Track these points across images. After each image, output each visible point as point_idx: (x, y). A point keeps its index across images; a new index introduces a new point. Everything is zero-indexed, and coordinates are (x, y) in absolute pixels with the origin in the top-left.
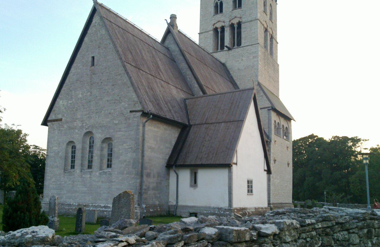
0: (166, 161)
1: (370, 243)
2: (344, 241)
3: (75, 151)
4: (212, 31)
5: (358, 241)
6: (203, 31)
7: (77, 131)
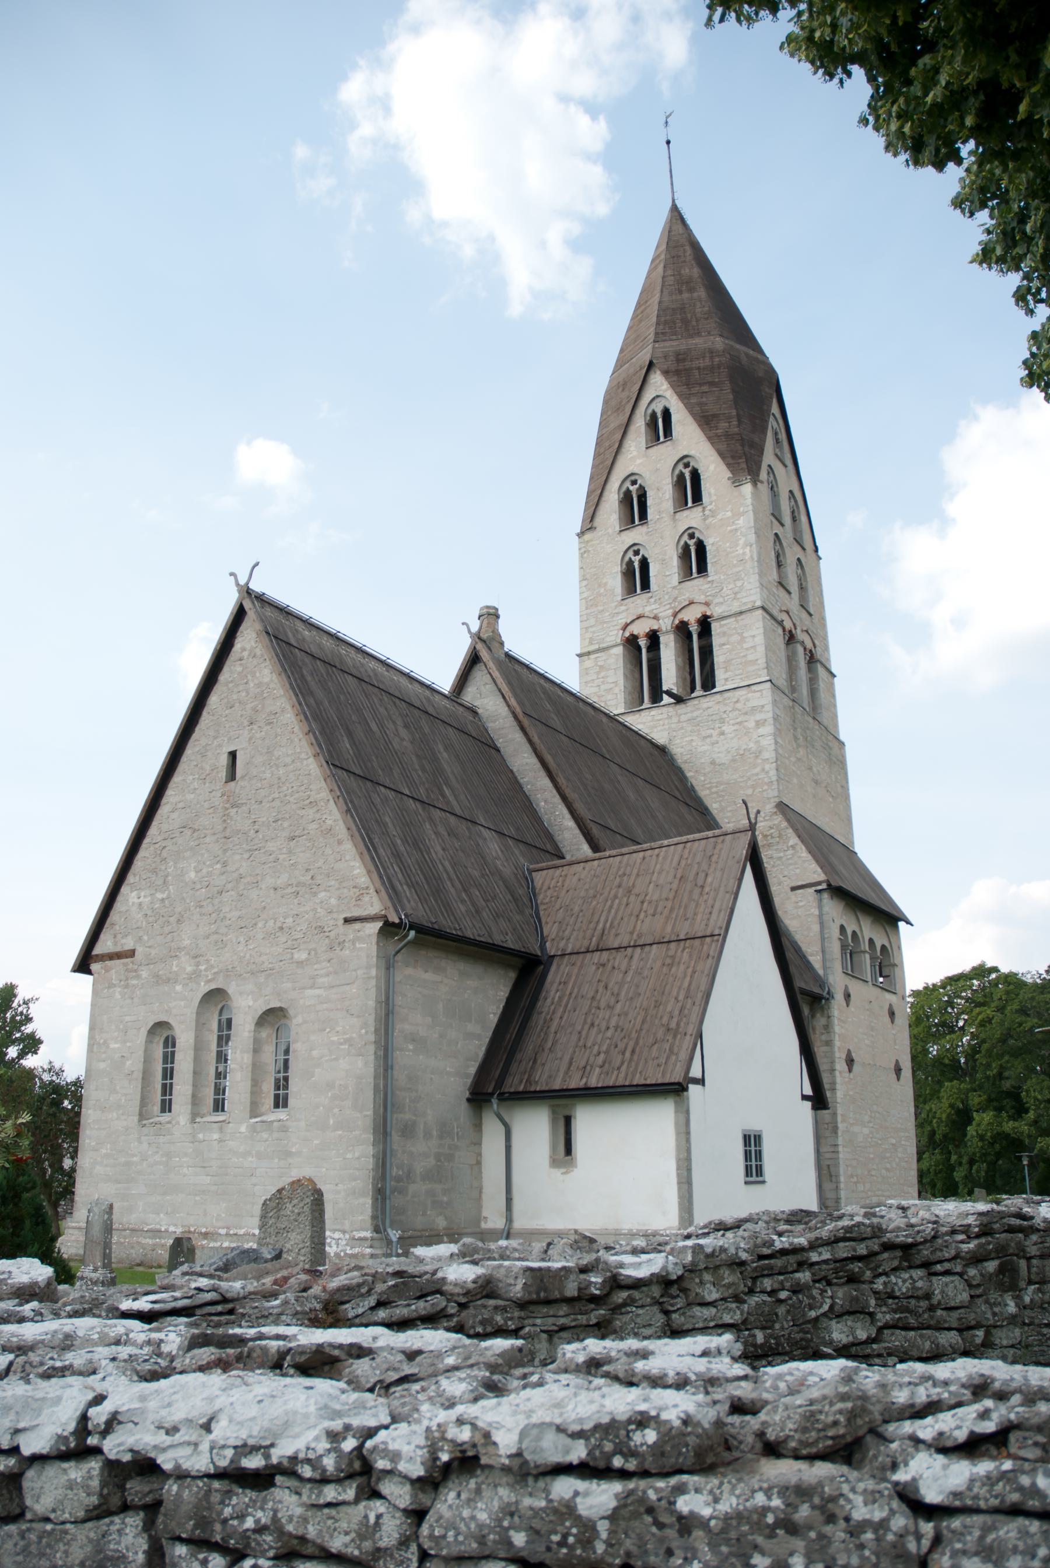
0: (469, 1081)
1: (1012, 1304)
2: (912, 1297)
3: (173, 1053)
5: (965, 1296)
7: (179, 988)
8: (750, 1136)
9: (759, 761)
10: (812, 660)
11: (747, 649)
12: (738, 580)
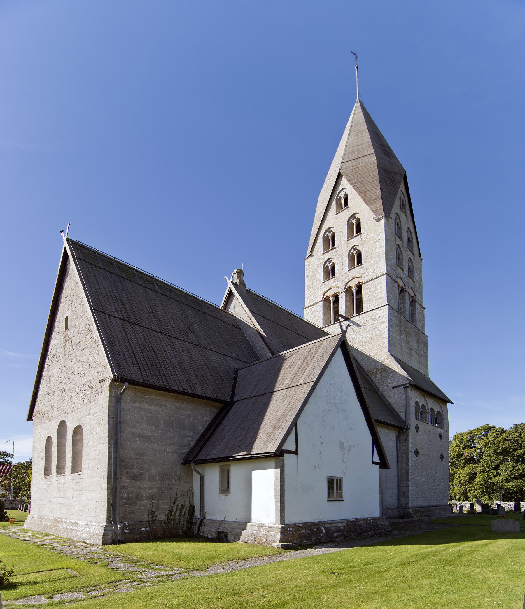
8: (333, 480)
9: (381, 339)
10: (413, 301)
11: (378, 293)
12: (376, 263)
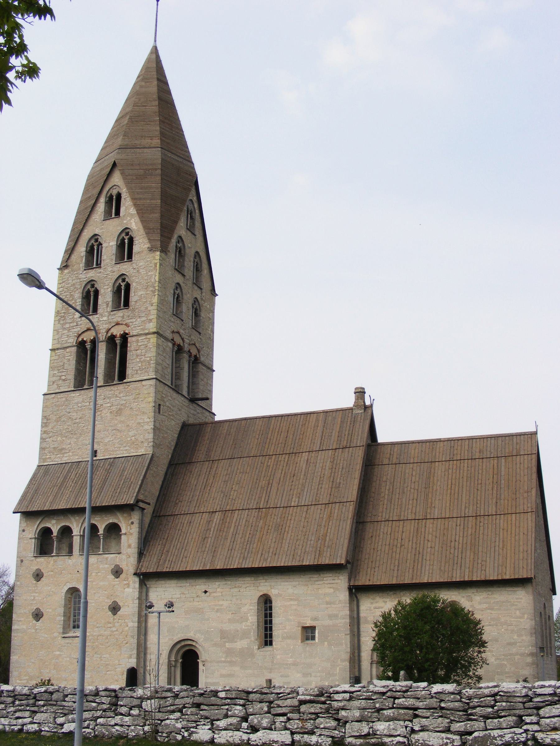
4: (76, 348)
6: (59, 346)
10: (195, 361)
